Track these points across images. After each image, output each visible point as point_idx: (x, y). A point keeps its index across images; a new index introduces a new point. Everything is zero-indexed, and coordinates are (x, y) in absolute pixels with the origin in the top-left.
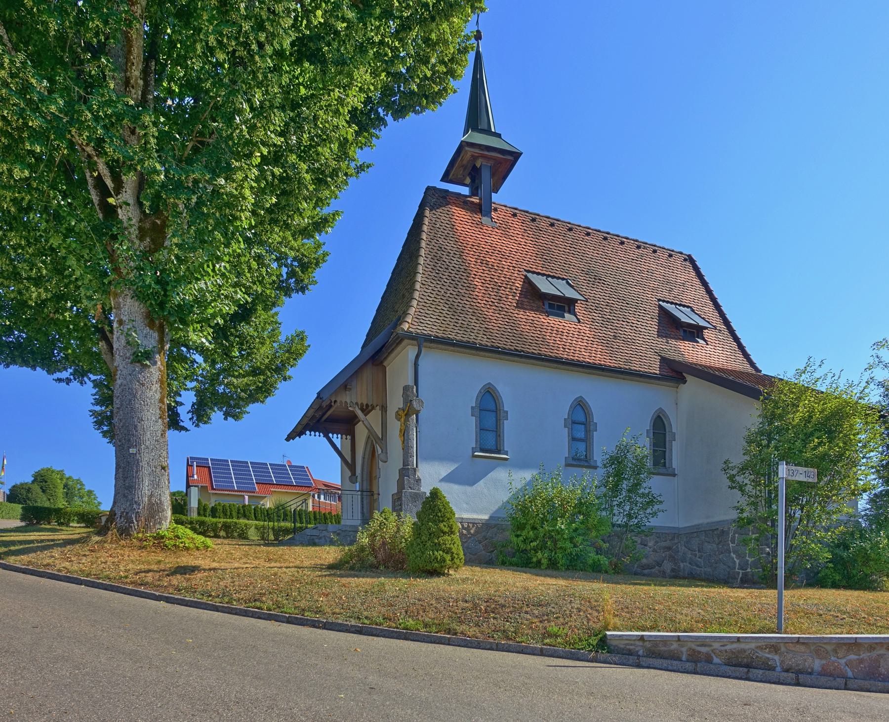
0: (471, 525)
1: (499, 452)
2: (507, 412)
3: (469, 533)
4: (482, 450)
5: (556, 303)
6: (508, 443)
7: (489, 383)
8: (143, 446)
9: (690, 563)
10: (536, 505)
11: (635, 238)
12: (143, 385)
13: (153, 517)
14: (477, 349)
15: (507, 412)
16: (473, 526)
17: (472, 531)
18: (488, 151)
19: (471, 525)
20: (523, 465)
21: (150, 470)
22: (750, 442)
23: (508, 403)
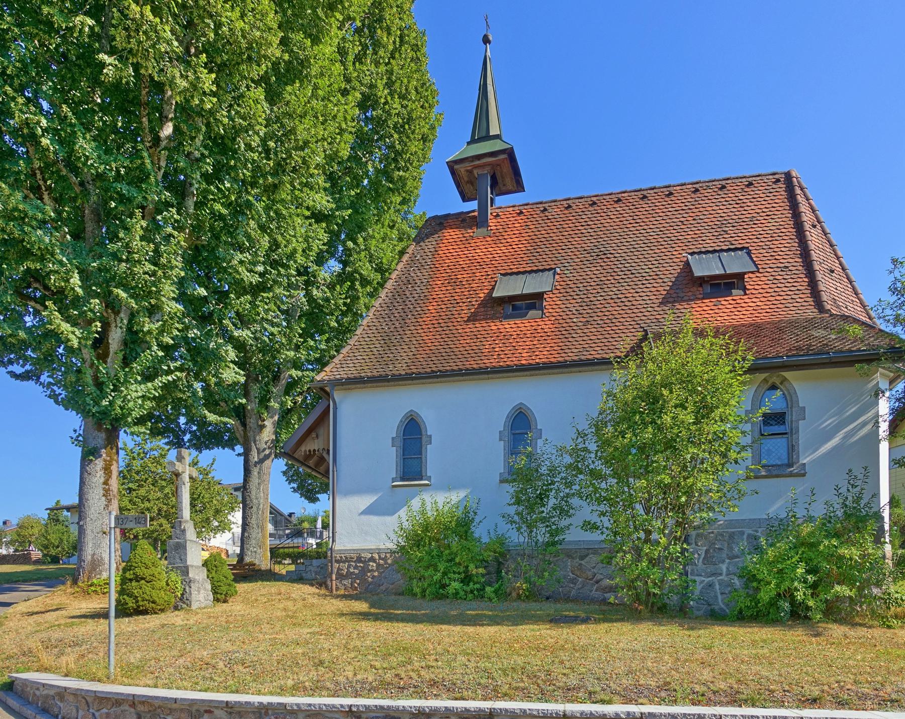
0: (388, 555)
1: (421, 479)
2: (430, 436)
3: (386, 563)
4: (402, 479)
5: (722, 282)
6: (431, 468)
7: (412, 411)
8: (88, 519)
9: (695, 581)
10: (607, 528)
11: (679, 182)
12: (90, 474)
13: (95, 570)
14: (488, 373)
15: (430, 436)
16: (391, 556)
17: (389, 561)
18: (479, 160)
19: (388, 555)
20: (450, 487)
21: (93, 536)
22: (73, 443)
23: (541, 420)
